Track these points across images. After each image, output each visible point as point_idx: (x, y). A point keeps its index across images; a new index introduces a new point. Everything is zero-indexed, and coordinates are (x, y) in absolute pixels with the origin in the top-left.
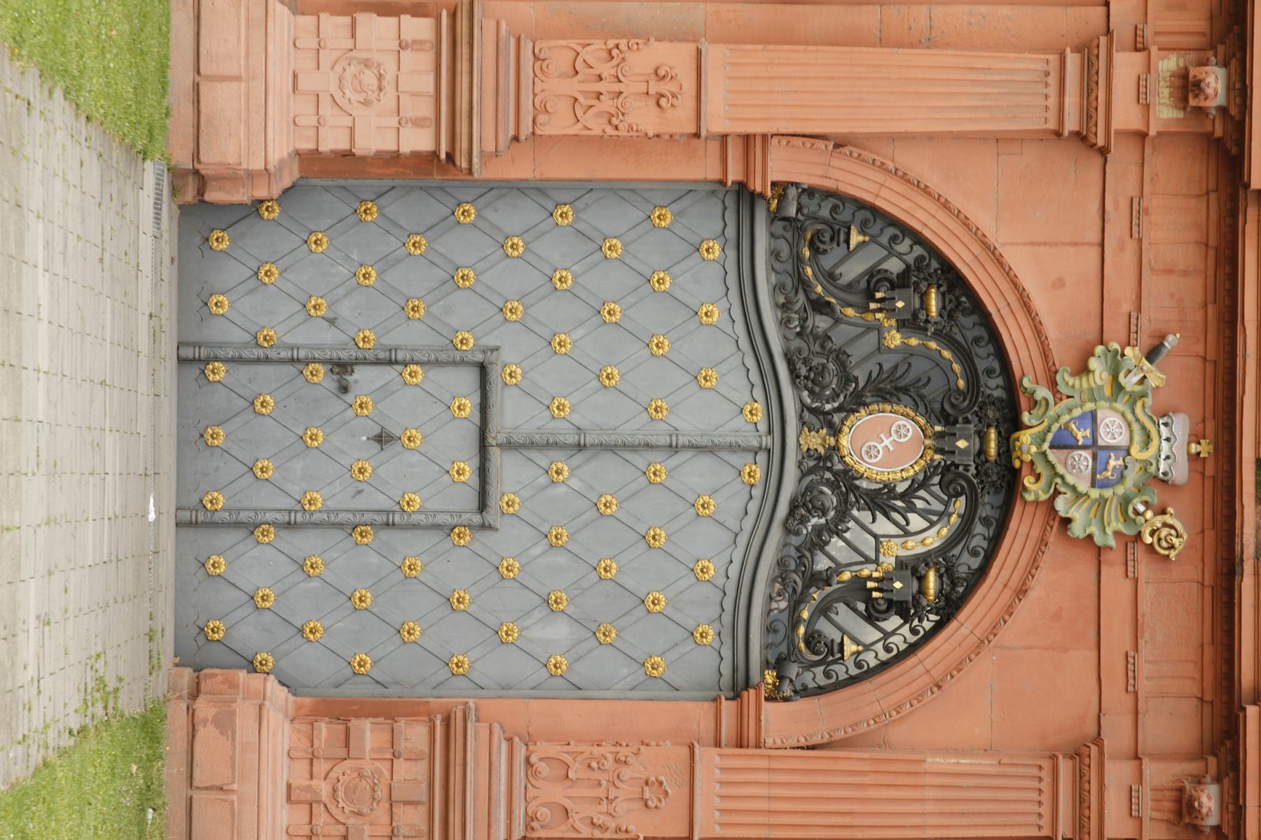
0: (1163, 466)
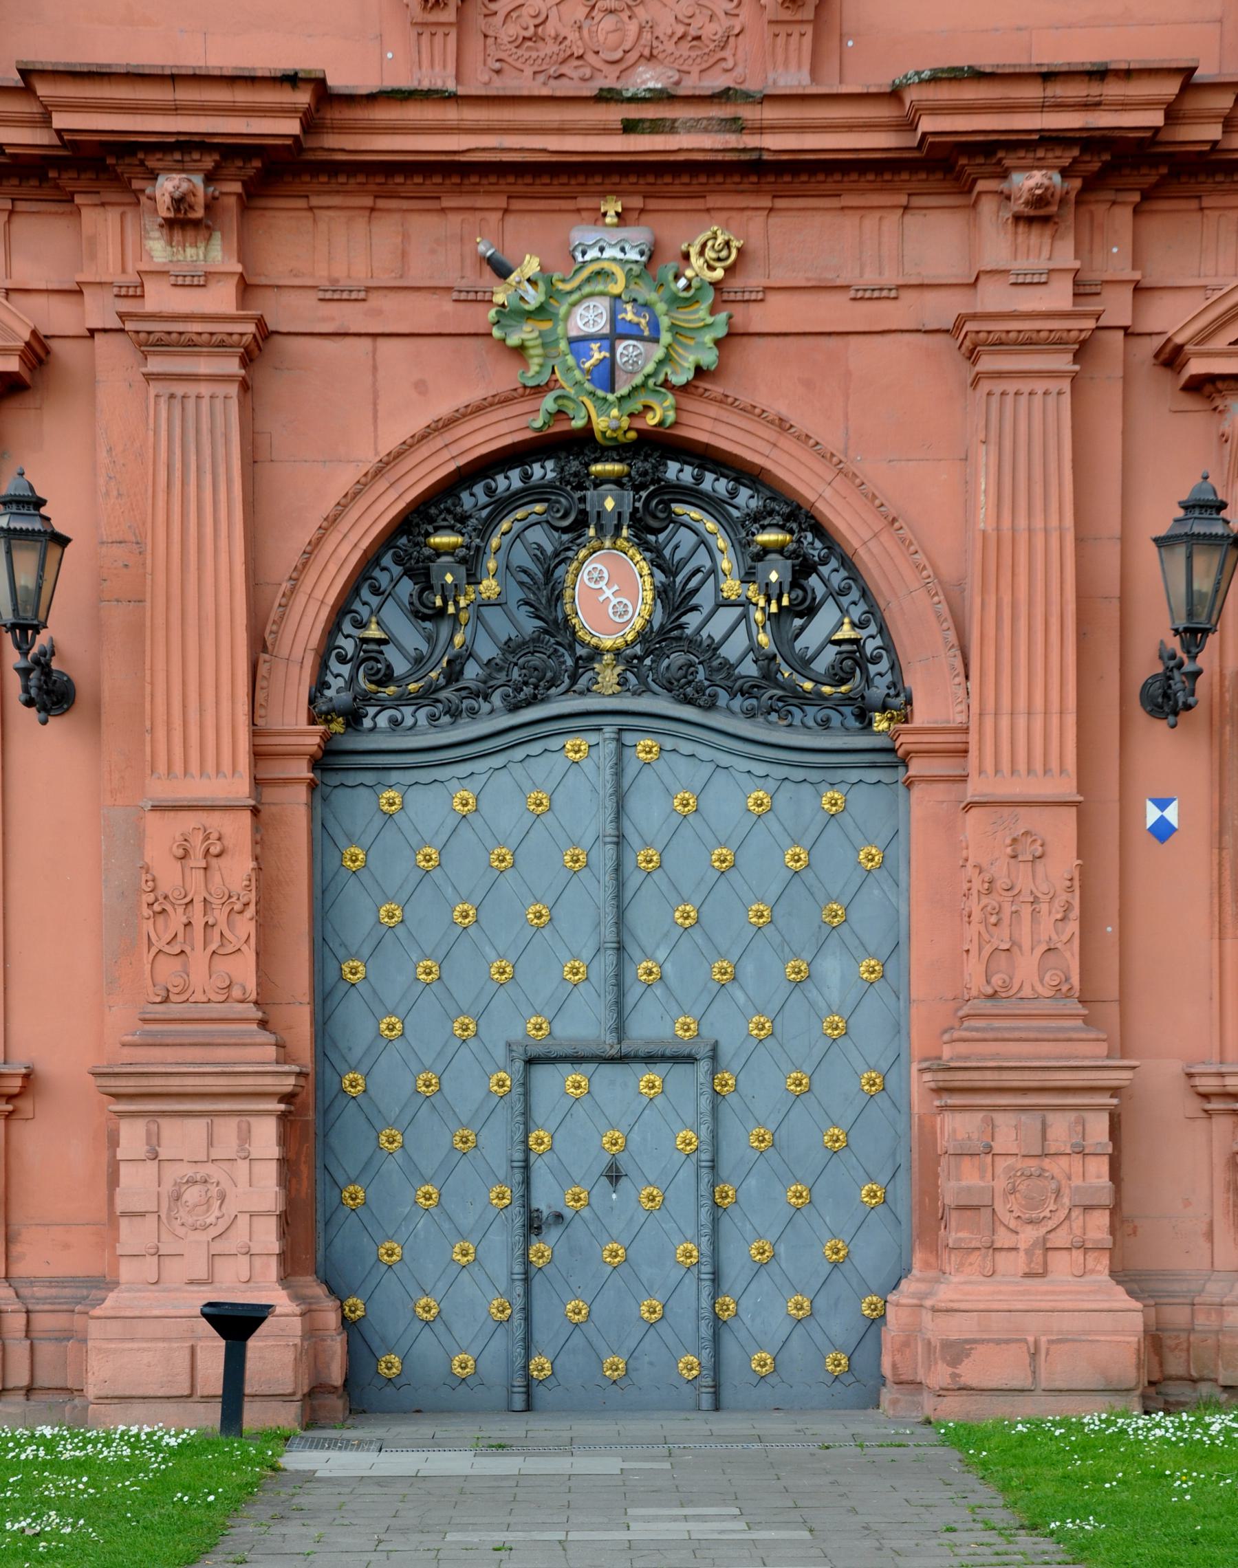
0: (633, 255)
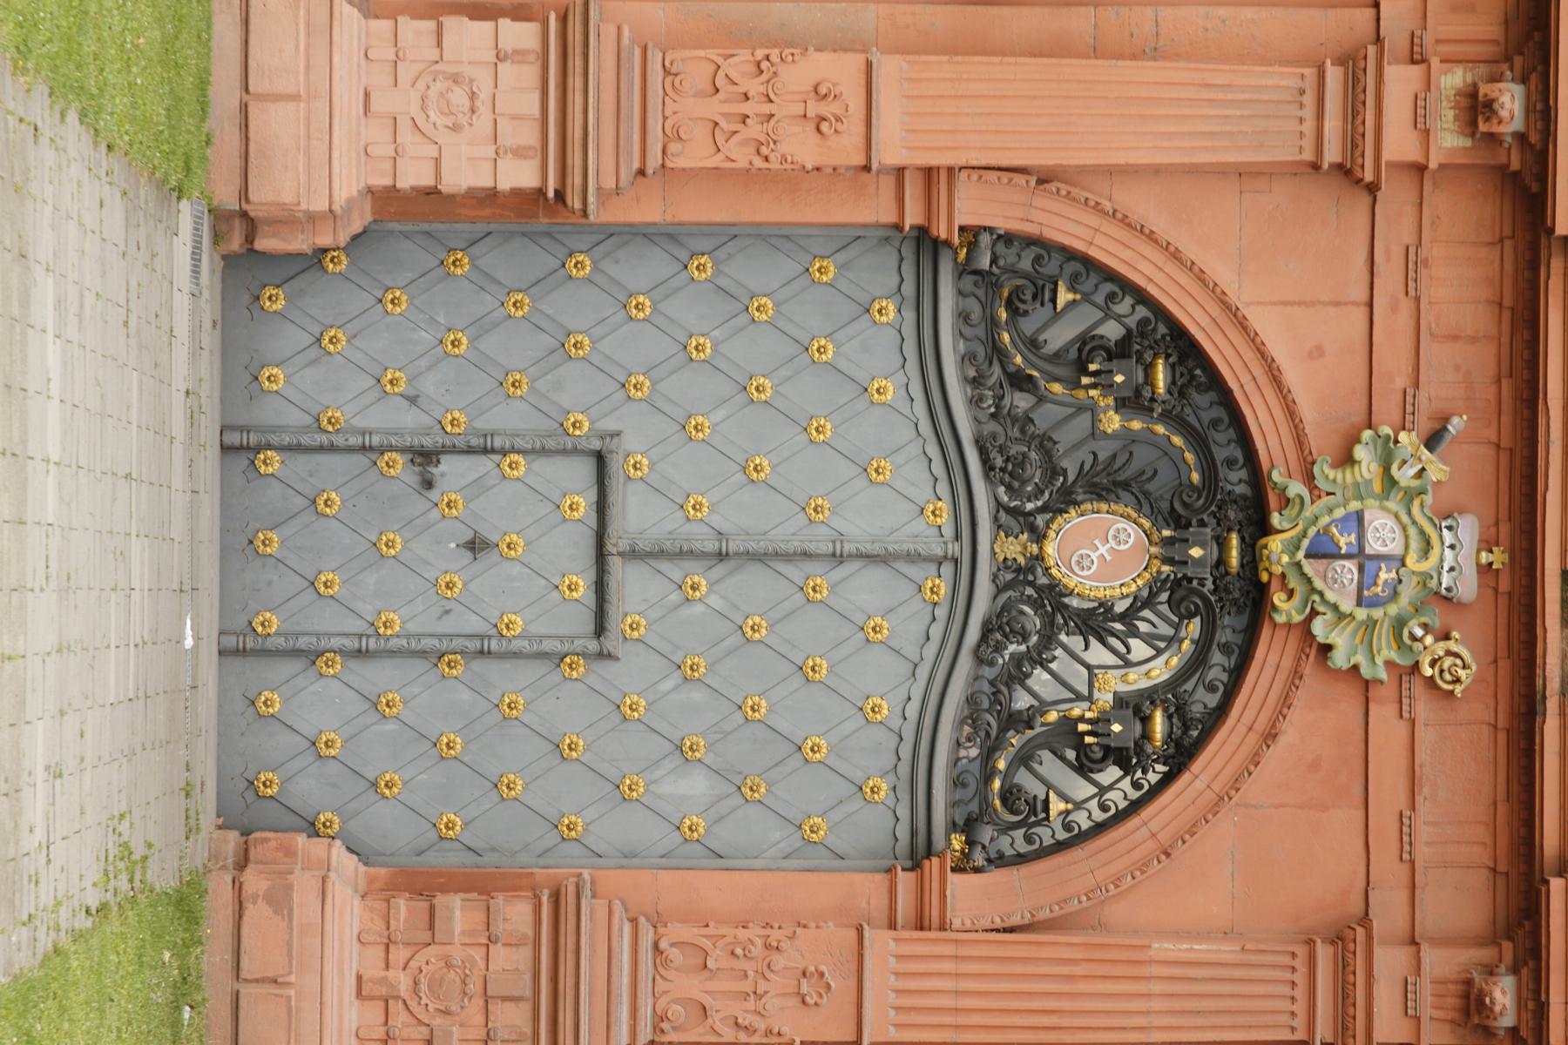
0: (1446, 580)
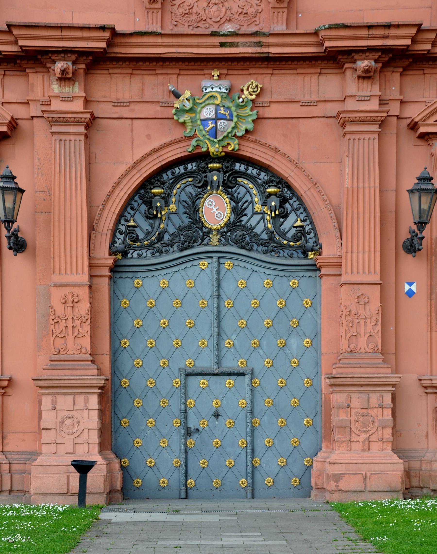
0: (223, 90)
